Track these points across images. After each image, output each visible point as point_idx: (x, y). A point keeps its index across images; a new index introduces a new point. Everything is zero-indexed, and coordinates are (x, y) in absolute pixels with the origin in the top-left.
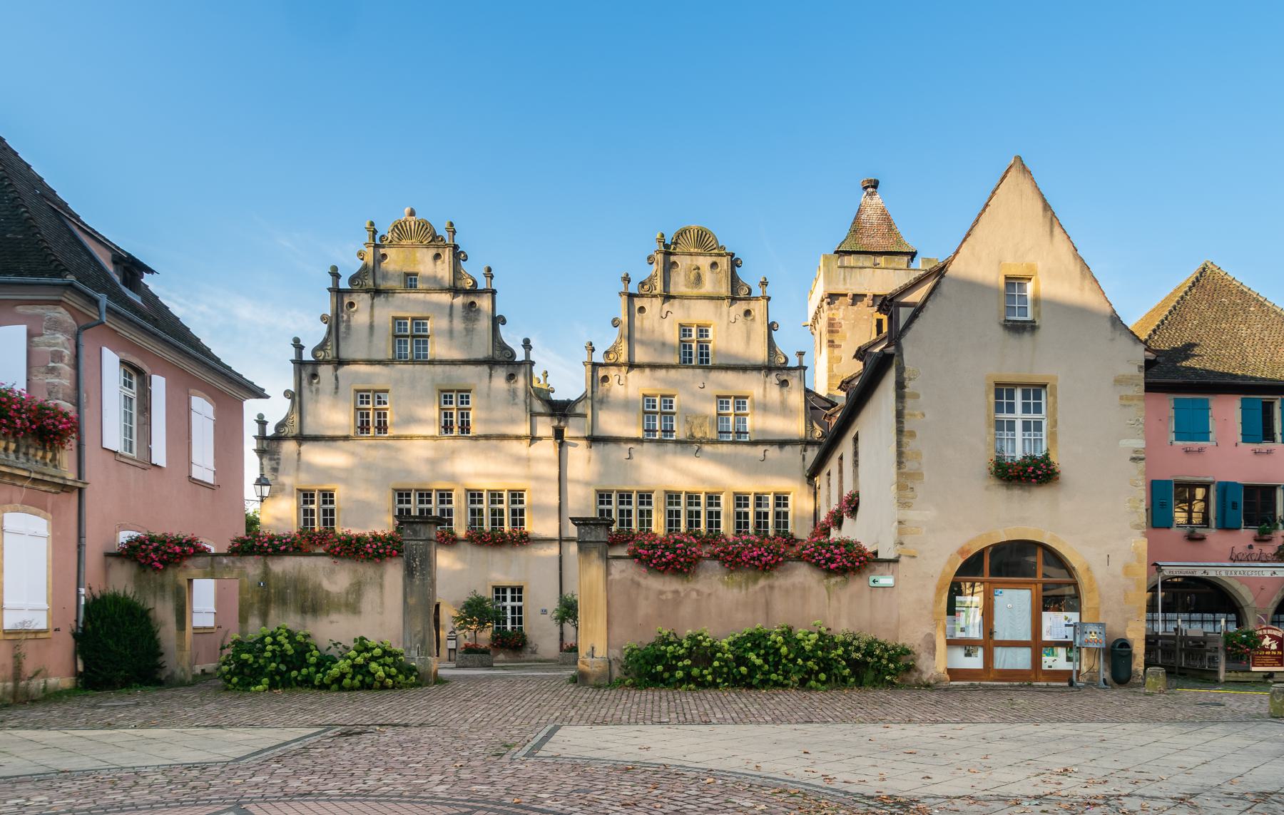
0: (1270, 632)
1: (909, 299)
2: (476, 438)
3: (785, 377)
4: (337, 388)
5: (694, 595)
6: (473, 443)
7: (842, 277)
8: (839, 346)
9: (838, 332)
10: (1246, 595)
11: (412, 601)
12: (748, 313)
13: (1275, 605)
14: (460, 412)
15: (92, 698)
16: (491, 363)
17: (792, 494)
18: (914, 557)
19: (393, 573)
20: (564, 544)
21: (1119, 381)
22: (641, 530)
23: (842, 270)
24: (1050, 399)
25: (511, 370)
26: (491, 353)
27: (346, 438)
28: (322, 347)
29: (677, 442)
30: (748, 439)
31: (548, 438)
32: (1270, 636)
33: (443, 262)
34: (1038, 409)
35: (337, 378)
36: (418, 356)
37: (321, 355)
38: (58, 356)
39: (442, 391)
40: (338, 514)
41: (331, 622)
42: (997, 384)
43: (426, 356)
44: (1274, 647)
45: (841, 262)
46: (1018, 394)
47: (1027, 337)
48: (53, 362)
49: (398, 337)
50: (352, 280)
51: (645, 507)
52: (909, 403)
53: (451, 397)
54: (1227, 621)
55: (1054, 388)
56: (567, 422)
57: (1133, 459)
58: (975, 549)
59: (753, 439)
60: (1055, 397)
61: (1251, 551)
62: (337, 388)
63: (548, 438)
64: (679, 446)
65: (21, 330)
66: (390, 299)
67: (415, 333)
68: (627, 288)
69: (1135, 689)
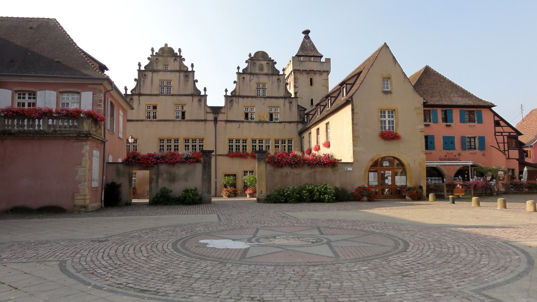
0: (459, 183)
1: (349, 82)
2: (188, 121)
3: (291, 101)
4: (139, 103)
5: (292, 174)
6: (186, 122)
7: (299, 64)
8: (298, 87)
9: (297, 82)
10: (445, 171)
11: (205, 177)
12: (278, 79)
13: (454, 174)
14: (176, 112)
15: (154, 209)
16: (192, 95)
17: (293, 140)
18: (358, 162)
19: (199, 167)
20: (217, 157)
21: (416, 108)
22: (236, 152)
23: (299, 62)
24: (396, 114)
25: (200, 98)
26: (193, 92)
27: (142, 121)
28: (134, 90)
29: (256, 122)
30: (278, 121)
31: (211, 121)
32: (459, 184)
33: (177, 61)
34: (392, 117)
35: (139, 100)
36: (168, 93)
37: (134, 92)
38: (100, 101)
39: (176, 105)
40: (139, 147)
41: (179, 184)
42: (381, 109)
43: (170, 93)
44: (461, 187)
45: (298, 59)
46: (387, 112)
47: (389, 95)
48: (99, 102)
49: (162, 87)
50: (145, 67)
51: (245, 144)
52: (355, 115)
53: (179, 107)
54: (431, 180)
55: (397, 111)
56: (218, 115)
57: (421, 132)
58: (376, 159)
59: (280, 121)
60: (398, 113)
61: (446, 157)
62: (139, 103)
63: (211, 121)
64: (256, 124)
65: (91, 93)
66: (158, 73)
67: (167, 85)
68: (238, 71)
69: (94, 209)
